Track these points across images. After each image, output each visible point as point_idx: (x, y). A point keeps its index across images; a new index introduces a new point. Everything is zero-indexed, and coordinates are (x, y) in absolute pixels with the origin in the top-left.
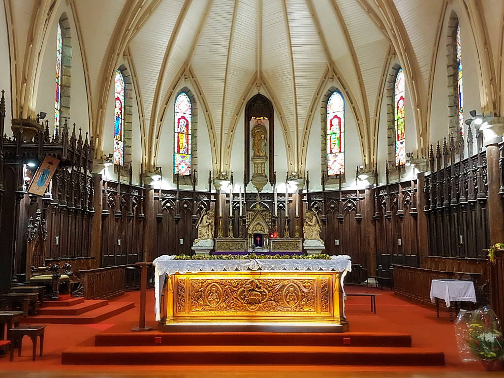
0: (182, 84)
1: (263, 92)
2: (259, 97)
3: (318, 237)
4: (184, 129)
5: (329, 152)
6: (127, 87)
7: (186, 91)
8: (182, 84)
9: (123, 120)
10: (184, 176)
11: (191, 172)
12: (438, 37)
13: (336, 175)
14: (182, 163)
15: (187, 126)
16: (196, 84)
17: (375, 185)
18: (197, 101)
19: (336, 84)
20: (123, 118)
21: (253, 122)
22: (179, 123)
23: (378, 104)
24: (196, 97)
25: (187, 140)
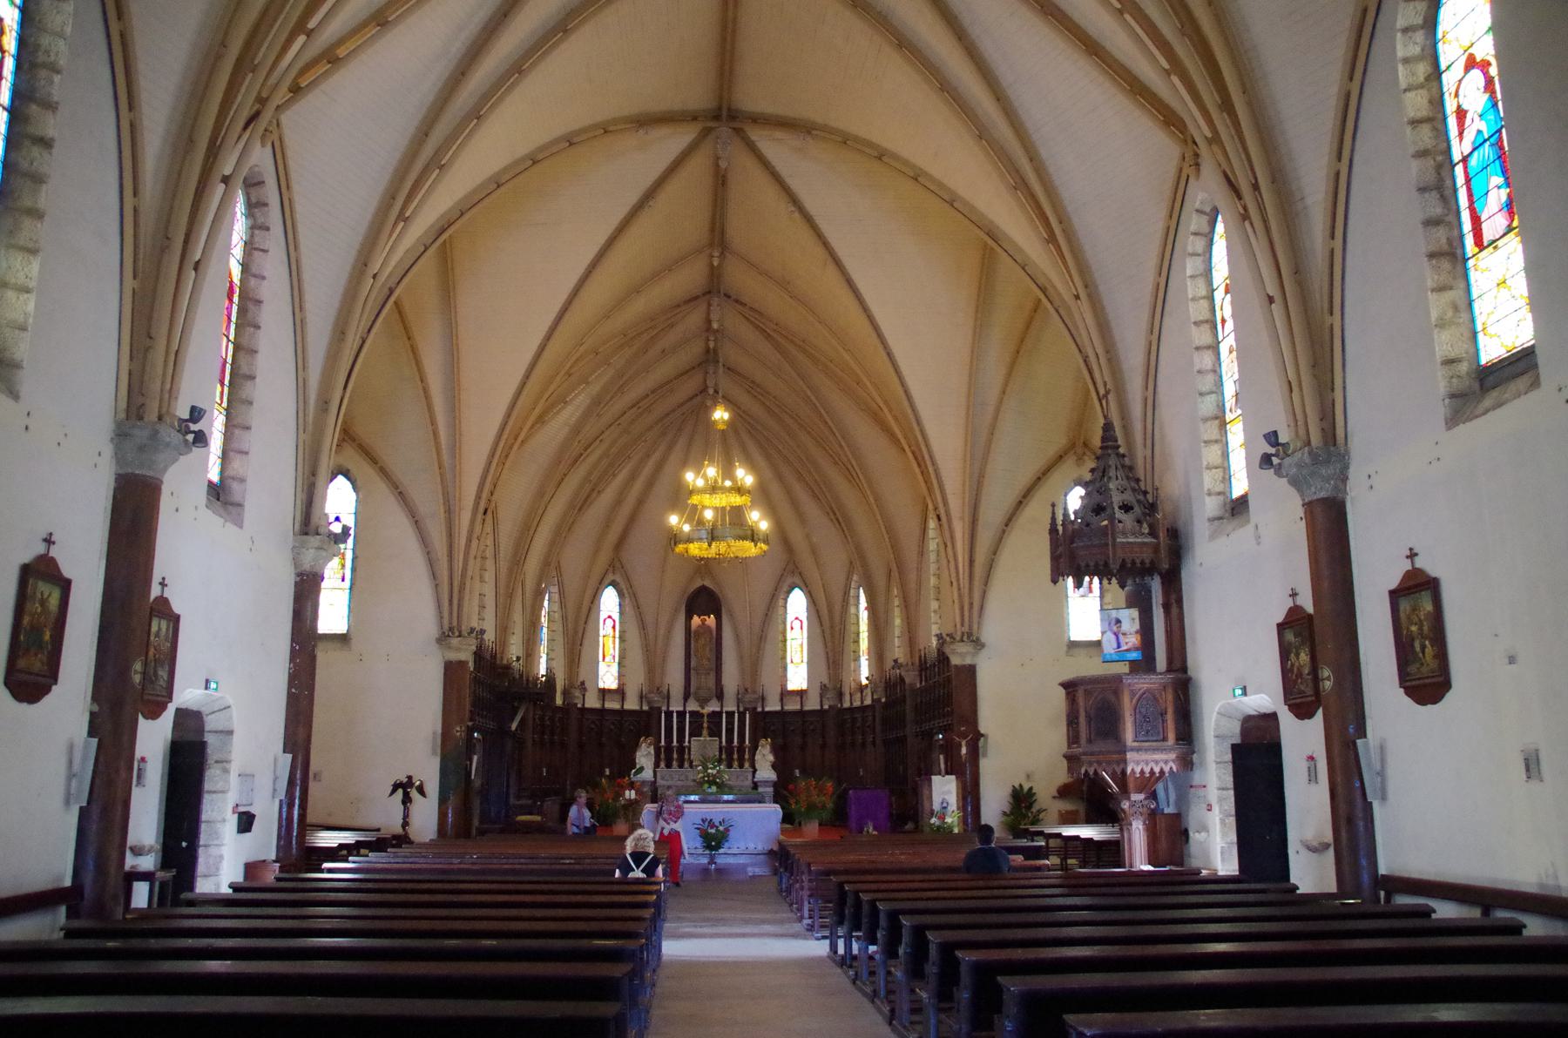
0: (610, 577)
1: (708, 583)
2: (703, 589)
3: (770, 768)
4: (611, 631)
5: (788, 661)
6: (256, 239)
7: (614, 584)
8: (610, 577)
9: (231, 346)
10: (610, 691)
11: (619, 684)
12: (1178, 205)
13: (798, 691)
14: (608, 674)
15: (614, 627)
16: (628, 579)
17: (839, 705)
18: (626, 595)
19: (797, 580)
20: (232, 337)
21: (696, 620)
22: (604, 623)
23: (1177, 188)
24: (625, 591)
25: (614, 643)
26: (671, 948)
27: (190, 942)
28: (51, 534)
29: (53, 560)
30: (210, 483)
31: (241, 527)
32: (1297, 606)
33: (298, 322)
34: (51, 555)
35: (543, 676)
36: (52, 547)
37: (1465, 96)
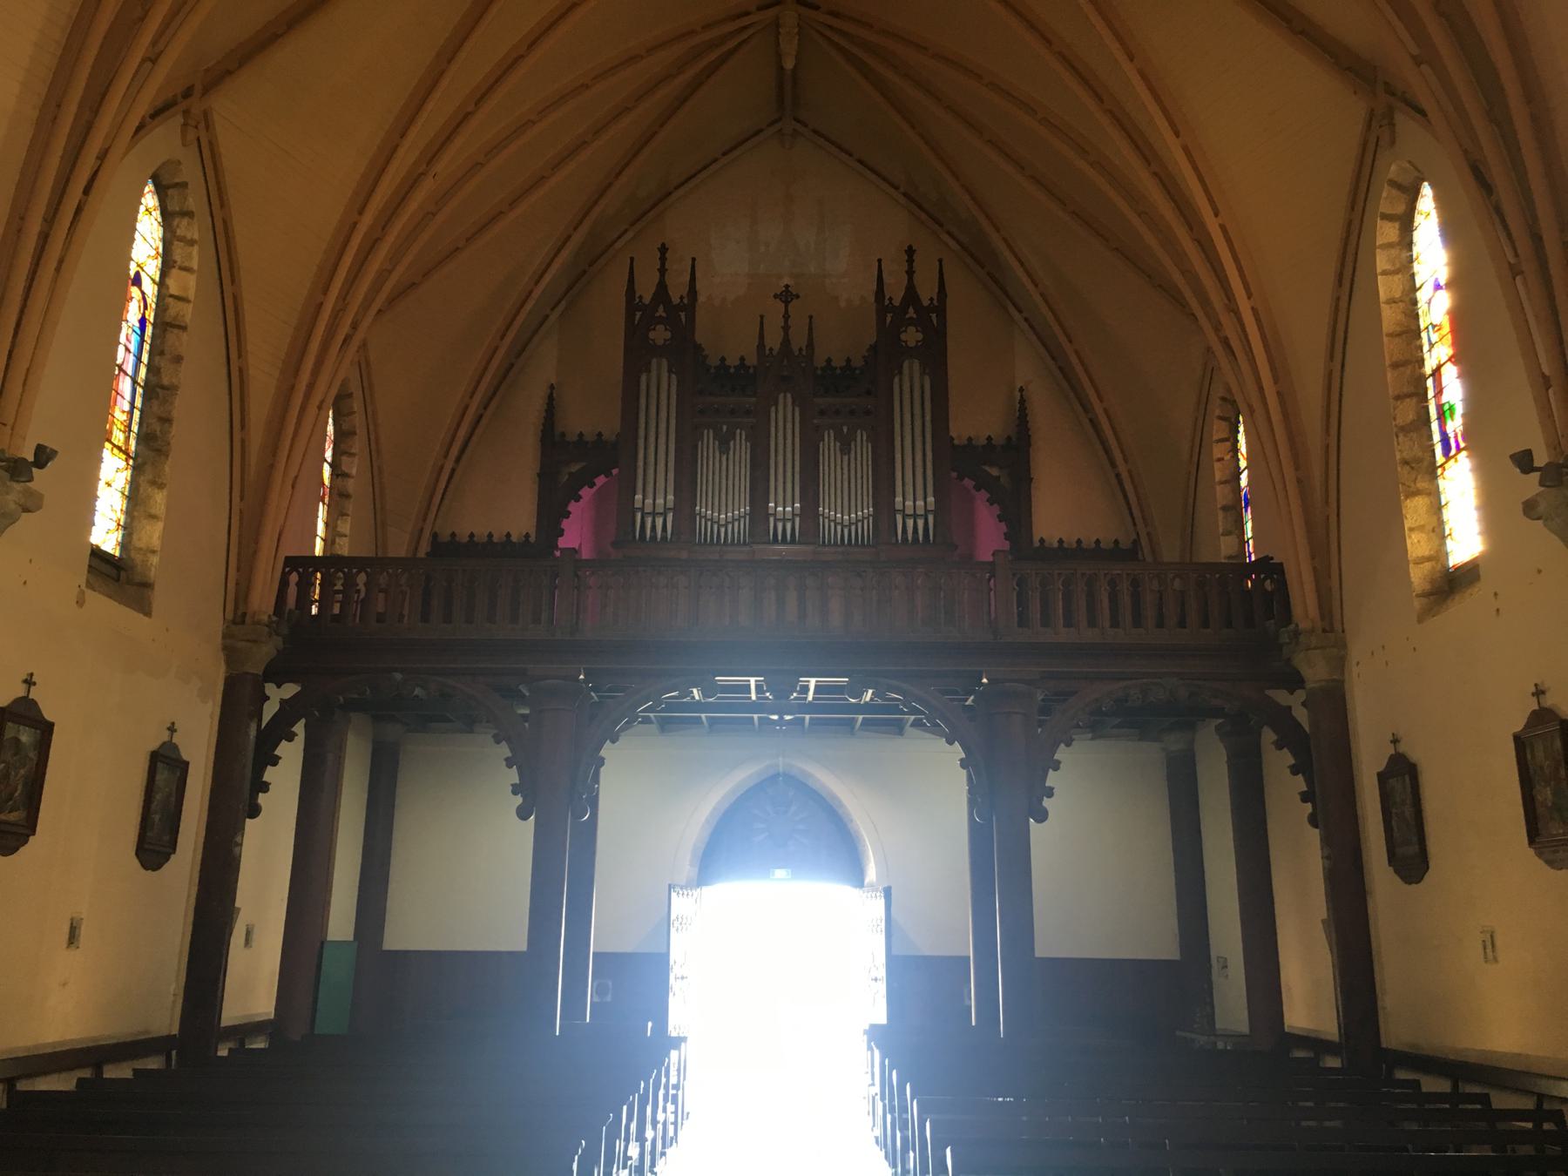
26: (317, 555)
27: (709, 534)
28: (32, 675)
29: (34, 703)
30: (97, 553)
31: (148, 614)
32: (1399, 753)
33: (229, 302)
34: (31, 697)
35: (1513, 1150)
36: (32, 688)
37: (282, 900)
